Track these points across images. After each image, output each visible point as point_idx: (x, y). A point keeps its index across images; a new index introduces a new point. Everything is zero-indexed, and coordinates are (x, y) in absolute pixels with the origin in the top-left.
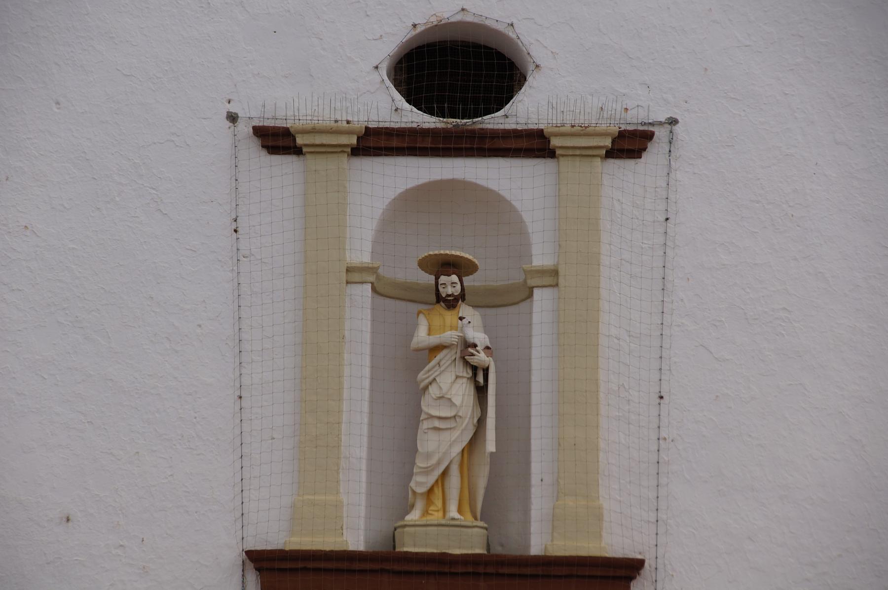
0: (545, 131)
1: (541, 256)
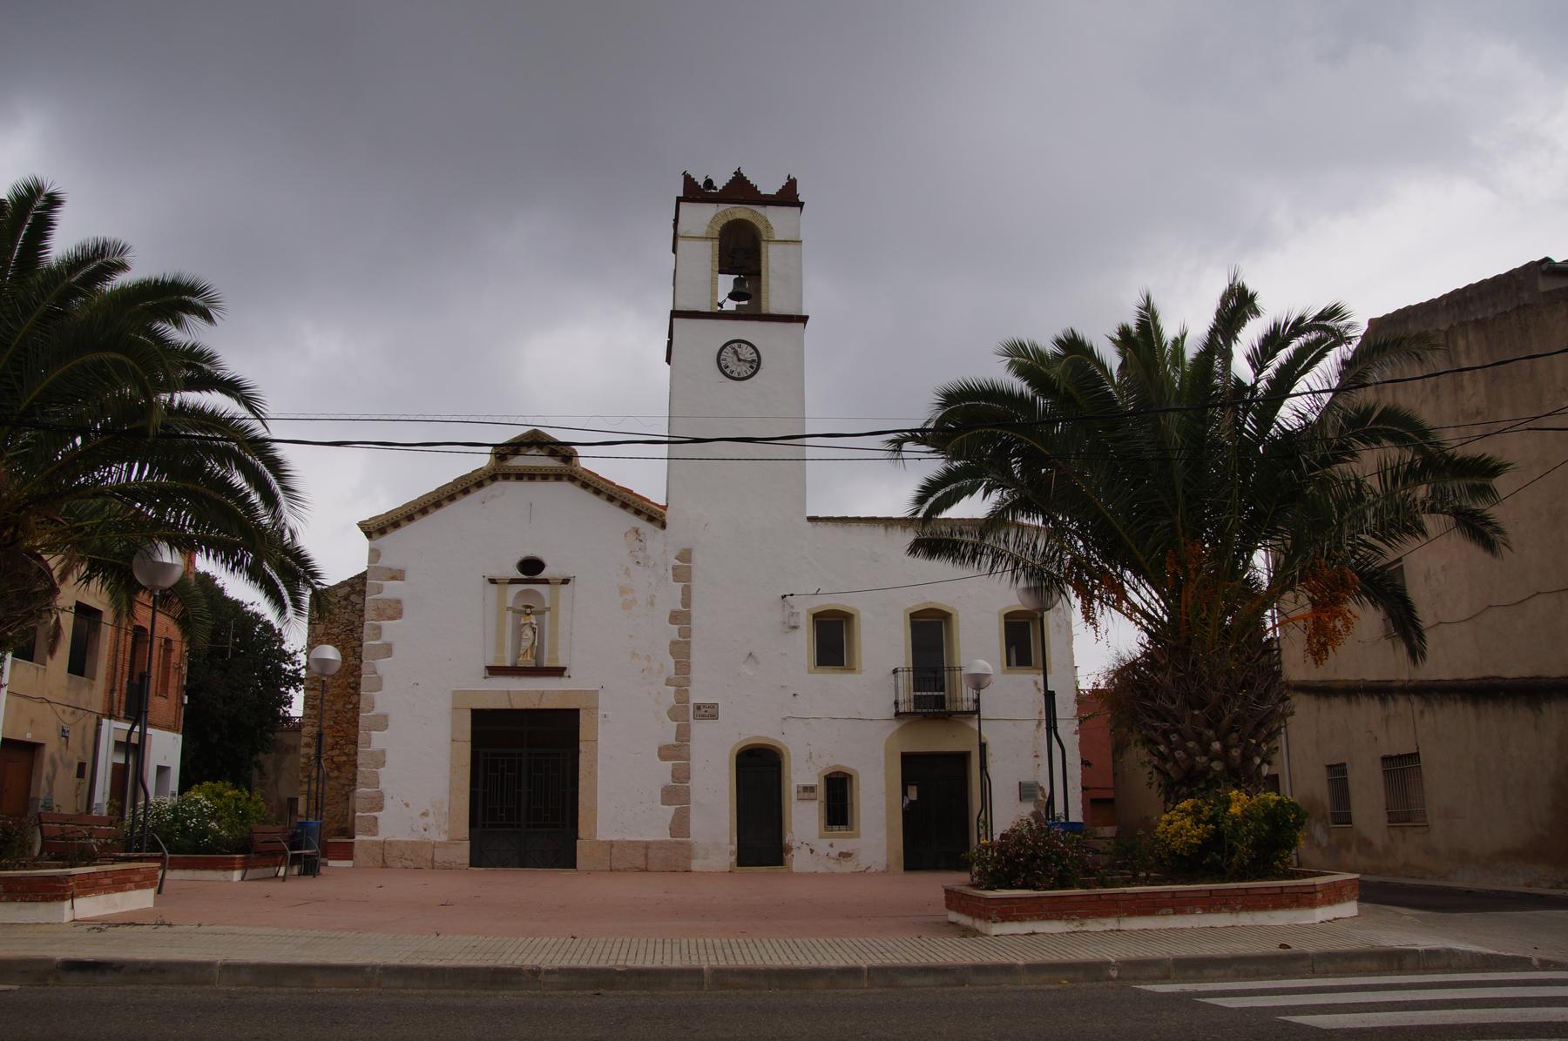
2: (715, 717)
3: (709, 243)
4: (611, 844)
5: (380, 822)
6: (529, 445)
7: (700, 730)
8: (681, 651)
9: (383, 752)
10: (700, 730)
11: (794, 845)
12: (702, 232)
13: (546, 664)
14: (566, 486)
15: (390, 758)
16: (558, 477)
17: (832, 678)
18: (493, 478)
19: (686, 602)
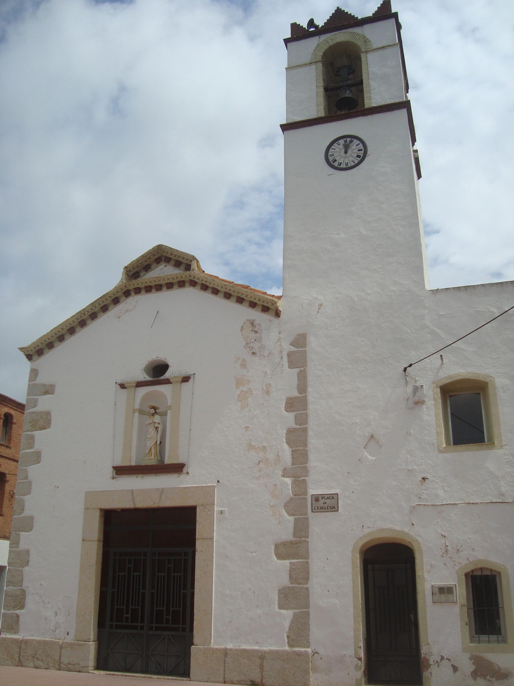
0: (37, 356)
1: (169, 403)
2: (334, 508)
3: (313, 67)
4: (226, 652)
5: (21, 619)
6: (158, 261)
7: (319, 524)
8: (297, 438)
9: (28, 552)
10: (319, 524)
11: (432, 660)
12: (307, 60)
13: (167, 461)
14: (189, 291)
15: (33, 558)
16: (182, 284)
17: (468, 455)
18: (127, 294)
19: (302, 387)
